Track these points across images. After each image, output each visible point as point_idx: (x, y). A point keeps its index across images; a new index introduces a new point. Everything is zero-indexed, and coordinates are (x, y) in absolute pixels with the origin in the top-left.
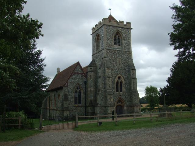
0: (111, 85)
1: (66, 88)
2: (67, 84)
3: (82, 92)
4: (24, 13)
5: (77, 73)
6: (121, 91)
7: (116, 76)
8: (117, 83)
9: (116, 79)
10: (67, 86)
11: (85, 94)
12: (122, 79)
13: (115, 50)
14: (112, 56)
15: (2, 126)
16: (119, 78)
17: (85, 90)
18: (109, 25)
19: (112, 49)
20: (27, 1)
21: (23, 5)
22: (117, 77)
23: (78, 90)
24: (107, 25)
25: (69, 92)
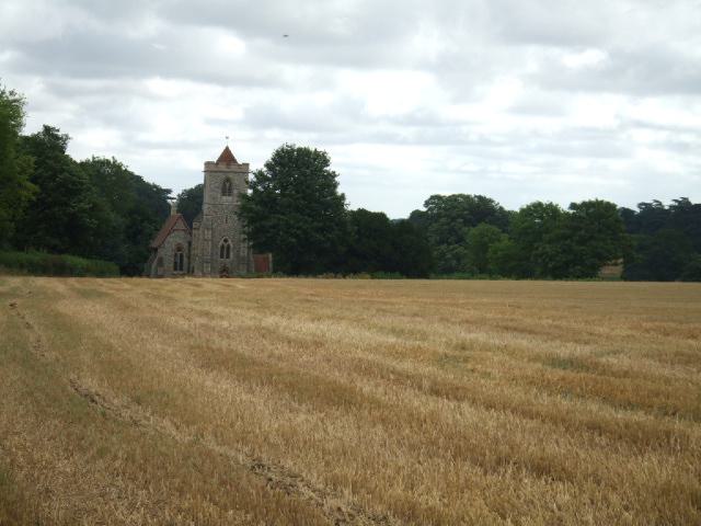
6: (228, 257)
8: (223, 247)
16: (226, 241)
20: (227, 149)
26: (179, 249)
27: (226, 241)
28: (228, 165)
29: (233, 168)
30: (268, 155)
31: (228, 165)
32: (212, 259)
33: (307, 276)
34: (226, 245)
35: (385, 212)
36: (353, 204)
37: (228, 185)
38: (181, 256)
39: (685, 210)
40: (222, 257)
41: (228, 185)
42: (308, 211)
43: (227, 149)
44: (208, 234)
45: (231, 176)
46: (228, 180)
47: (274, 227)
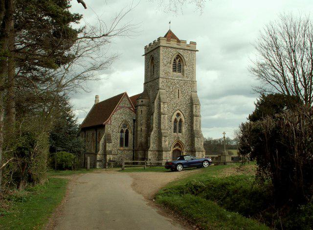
2: (111, 122)
3: (130, 131)
6: (180, 131)
8: (176, 120)
9: (174, 117)
11: (134, 134)
14: (169, 87)
16: (178, 115)
22: (175, 114)
24: (164, 47)
34: (178, 120)
40: (175, 131)
45: (181, 52)
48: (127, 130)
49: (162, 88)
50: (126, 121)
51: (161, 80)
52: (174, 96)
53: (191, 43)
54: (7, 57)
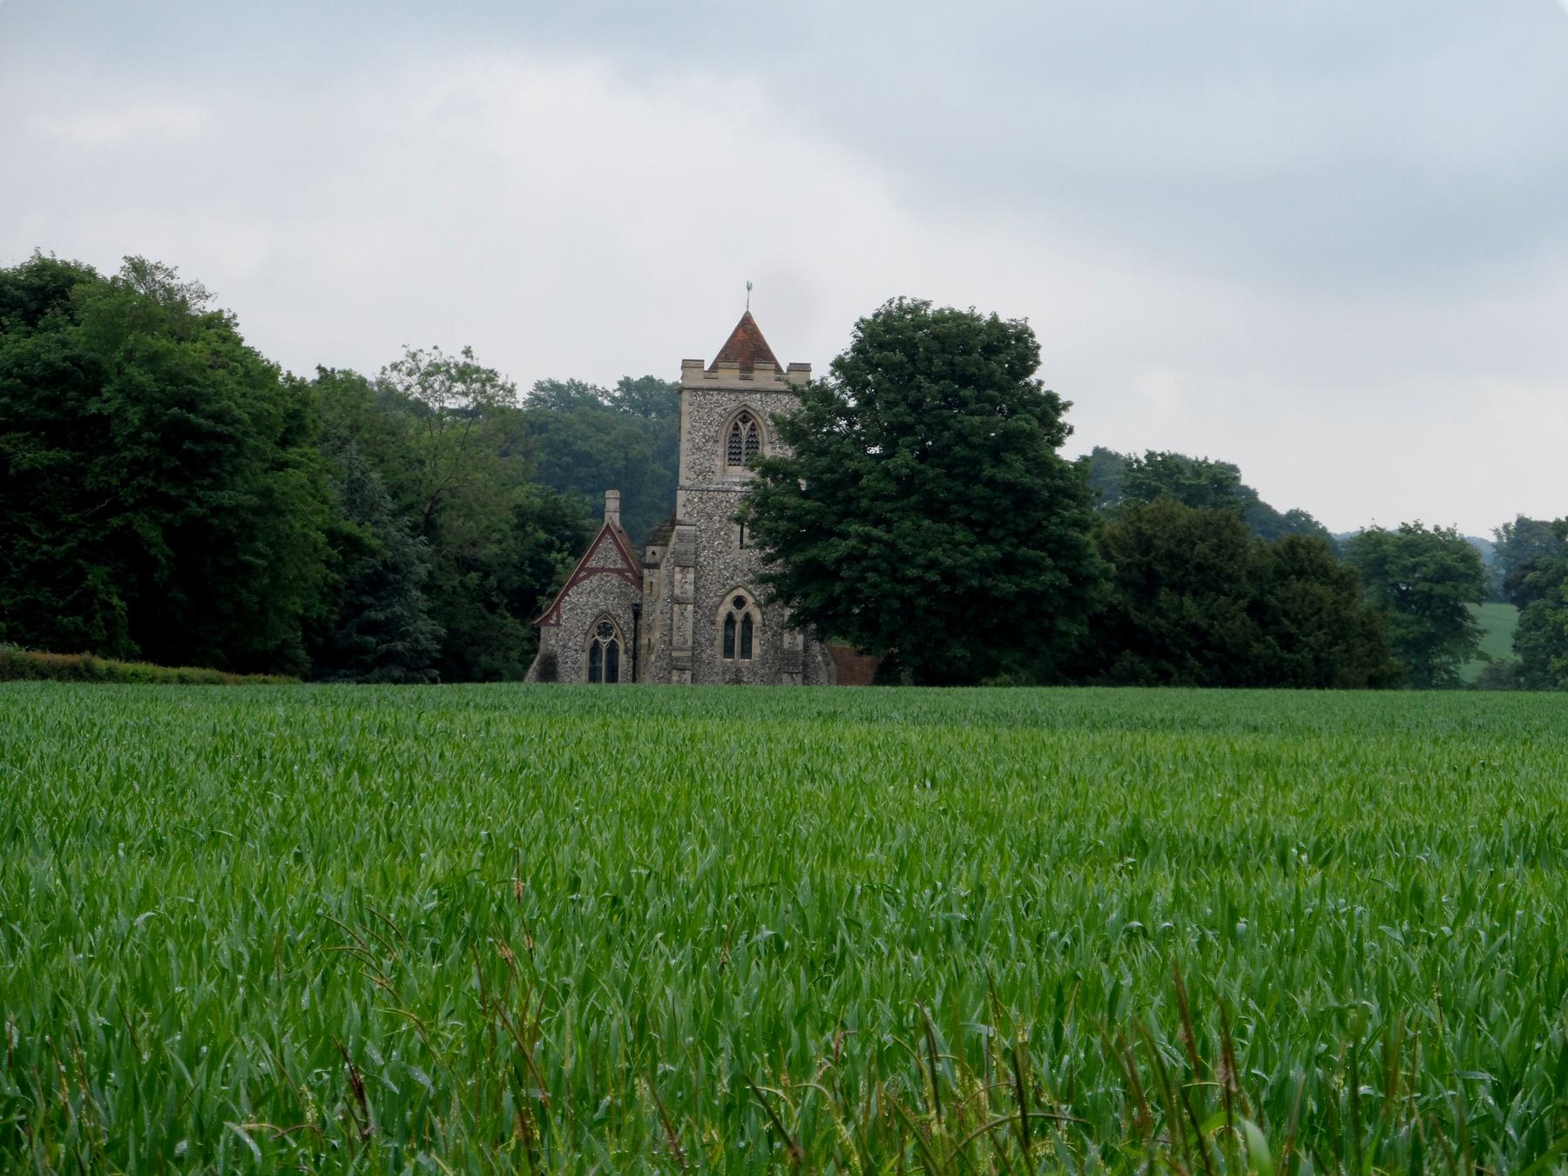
0: (689, 633)
1: (553, 630)
2: (559, 616)
3: (621, 648)
4: (1033, 379)
5: (603, 570)
6: (746, 652)
7: (724, 597)
8: (730, 620)
9: (727, 607)
10: (558, 624)
11: (635, 657)
12: (750, 606)
13: (727, 491)
14: (710, 517)
15: (693, 680)
16: (739, 602)
17: (635, 640)
18: (702, 389)
19: (713, 487)
20: (747, 324)
21: (1044, 389)
22: (729, 598)
23: (604, 642)
24: (695, 389)
25: (564, 646)
26: (605, 630)
27: (739, 602)
28: (747, 369)
29: (762, 378)
30: (843, 342)
31: (747, 369)
32: (694, 659)
33: (1267, 686)
34: (739, 616)
35: (1304, 508)
36: (1243, 482)
37: (744, 430)
38: (613, 648)
39: (1563, 528)
40: (728, 651)
41: (744, 430)
42: (963, 512)
43: (747, 324)
44: (685, 582)
45: (754, 402)
46: (745, 416)
47: (852, 558)
48: (613, 643)
49: (687, 519)
50: (604, 614)
51: (681, 496)
52: (727, 543)
53: (794, 367)
54: (679, 1154)
